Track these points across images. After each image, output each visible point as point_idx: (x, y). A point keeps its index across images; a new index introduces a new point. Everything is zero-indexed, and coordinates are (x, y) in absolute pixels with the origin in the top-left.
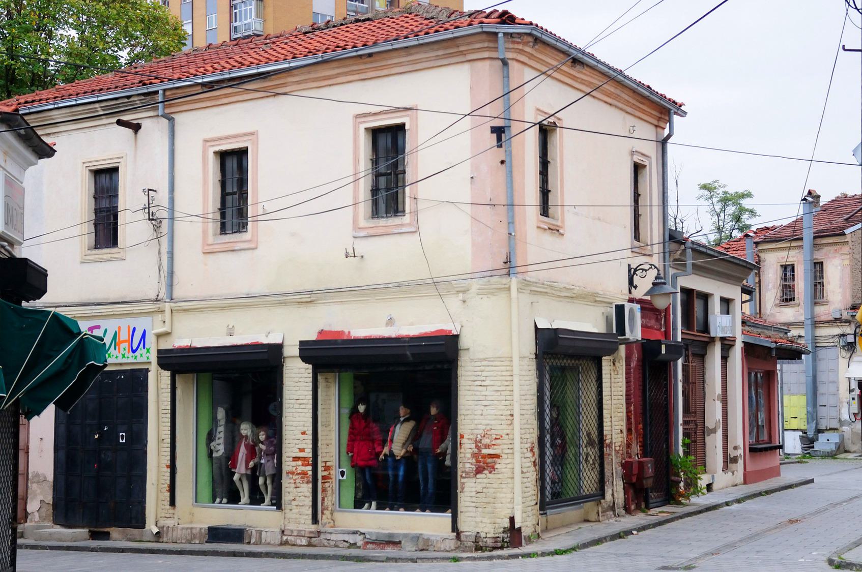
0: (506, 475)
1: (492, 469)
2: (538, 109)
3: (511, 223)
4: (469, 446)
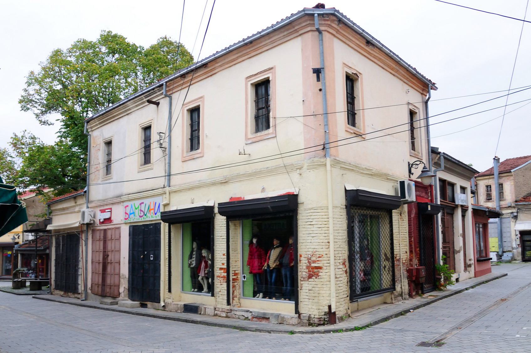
0: (326, 280)
1: (317, 275)
2: (344, 64)
3: (326, 125)
4: (305, 262)
